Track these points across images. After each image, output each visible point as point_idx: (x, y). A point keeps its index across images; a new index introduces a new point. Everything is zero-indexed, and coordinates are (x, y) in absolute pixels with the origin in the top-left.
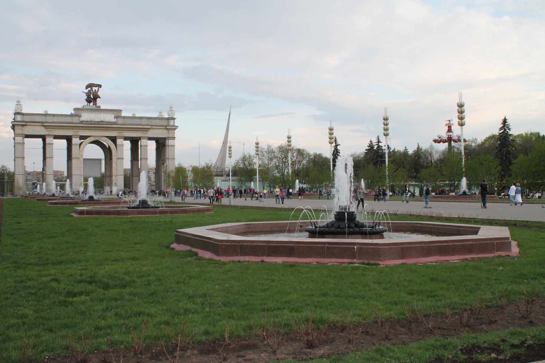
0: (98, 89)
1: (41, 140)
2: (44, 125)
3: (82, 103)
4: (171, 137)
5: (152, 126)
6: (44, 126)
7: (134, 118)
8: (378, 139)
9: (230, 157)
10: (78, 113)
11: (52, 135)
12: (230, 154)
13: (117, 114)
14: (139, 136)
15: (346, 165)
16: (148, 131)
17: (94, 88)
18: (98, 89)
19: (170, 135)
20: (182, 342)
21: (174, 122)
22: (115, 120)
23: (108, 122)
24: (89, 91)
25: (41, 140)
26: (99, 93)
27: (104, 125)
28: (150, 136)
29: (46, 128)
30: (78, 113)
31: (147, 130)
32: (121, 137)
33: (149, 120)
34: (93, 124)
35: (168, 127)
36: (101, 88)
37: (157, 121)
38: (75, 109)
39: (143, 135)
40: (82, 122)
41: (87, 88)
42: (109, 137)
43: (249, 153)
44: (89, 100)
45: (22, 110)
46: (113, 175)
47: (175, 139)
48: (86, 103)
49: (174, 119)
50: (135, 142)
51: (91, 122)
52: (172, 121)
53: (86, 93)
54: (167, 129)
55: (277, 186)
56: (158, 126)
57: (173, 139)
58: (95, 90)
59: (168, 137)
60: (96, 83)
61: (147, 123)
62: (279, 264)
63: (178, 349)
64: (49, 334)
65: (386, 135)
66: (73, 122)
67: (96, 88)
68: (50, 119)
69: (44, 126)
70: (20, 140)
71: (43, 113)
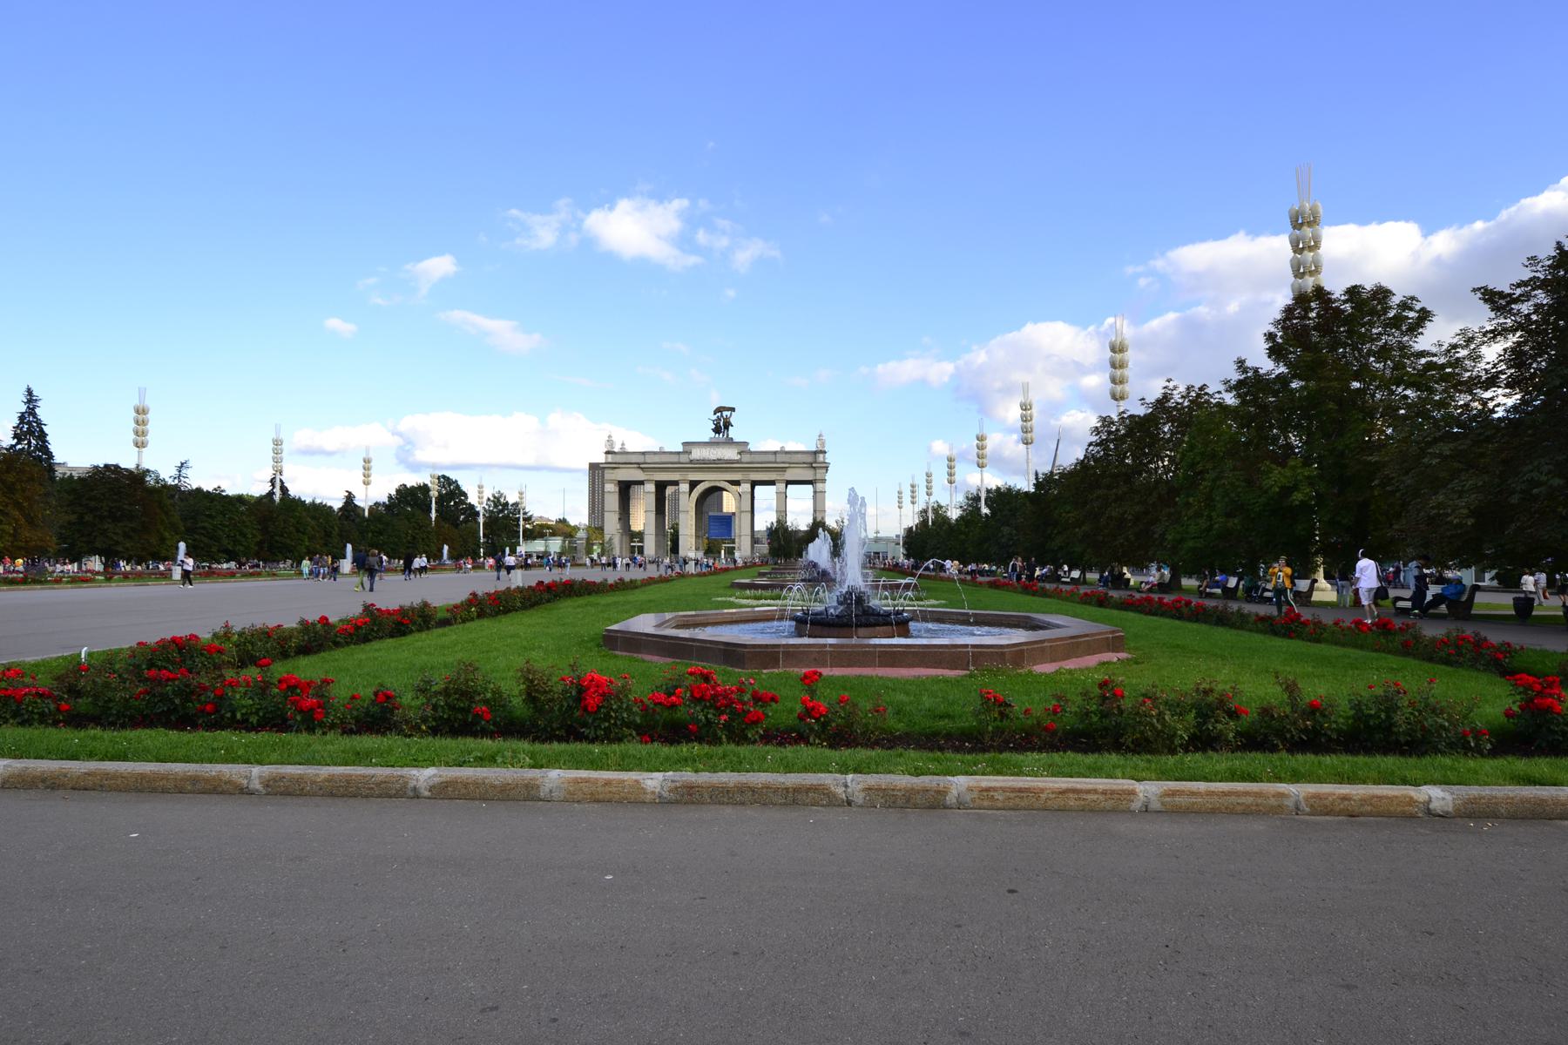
0: (731, 415)
1: (757, 487)
2: (639, 466)
3: (707, 434)
6: (642, 468)
8: (31, 411)
9: (913, 503)
10: (688, 448)
13: (742, 449)
16: (785, 471)
17: (725, 413)
18: (731, 415)
21: (824, 458)
25: (757, 487)
26: (732, 420)
30: (688, 448)
31: (784, 469)
35: (814, 465)
38: (685, 444)
39: (778, 478)
40: (691, 462)
41: (715, 414)
42: (699, 482)
44: (717, 430)
48: (714, 433)
49: (825, 452)
51: (704, 461)
52: (821, 456)
66: (681, 461)
67: (728, 413)
68: (649, 459)
69: (642, 468)
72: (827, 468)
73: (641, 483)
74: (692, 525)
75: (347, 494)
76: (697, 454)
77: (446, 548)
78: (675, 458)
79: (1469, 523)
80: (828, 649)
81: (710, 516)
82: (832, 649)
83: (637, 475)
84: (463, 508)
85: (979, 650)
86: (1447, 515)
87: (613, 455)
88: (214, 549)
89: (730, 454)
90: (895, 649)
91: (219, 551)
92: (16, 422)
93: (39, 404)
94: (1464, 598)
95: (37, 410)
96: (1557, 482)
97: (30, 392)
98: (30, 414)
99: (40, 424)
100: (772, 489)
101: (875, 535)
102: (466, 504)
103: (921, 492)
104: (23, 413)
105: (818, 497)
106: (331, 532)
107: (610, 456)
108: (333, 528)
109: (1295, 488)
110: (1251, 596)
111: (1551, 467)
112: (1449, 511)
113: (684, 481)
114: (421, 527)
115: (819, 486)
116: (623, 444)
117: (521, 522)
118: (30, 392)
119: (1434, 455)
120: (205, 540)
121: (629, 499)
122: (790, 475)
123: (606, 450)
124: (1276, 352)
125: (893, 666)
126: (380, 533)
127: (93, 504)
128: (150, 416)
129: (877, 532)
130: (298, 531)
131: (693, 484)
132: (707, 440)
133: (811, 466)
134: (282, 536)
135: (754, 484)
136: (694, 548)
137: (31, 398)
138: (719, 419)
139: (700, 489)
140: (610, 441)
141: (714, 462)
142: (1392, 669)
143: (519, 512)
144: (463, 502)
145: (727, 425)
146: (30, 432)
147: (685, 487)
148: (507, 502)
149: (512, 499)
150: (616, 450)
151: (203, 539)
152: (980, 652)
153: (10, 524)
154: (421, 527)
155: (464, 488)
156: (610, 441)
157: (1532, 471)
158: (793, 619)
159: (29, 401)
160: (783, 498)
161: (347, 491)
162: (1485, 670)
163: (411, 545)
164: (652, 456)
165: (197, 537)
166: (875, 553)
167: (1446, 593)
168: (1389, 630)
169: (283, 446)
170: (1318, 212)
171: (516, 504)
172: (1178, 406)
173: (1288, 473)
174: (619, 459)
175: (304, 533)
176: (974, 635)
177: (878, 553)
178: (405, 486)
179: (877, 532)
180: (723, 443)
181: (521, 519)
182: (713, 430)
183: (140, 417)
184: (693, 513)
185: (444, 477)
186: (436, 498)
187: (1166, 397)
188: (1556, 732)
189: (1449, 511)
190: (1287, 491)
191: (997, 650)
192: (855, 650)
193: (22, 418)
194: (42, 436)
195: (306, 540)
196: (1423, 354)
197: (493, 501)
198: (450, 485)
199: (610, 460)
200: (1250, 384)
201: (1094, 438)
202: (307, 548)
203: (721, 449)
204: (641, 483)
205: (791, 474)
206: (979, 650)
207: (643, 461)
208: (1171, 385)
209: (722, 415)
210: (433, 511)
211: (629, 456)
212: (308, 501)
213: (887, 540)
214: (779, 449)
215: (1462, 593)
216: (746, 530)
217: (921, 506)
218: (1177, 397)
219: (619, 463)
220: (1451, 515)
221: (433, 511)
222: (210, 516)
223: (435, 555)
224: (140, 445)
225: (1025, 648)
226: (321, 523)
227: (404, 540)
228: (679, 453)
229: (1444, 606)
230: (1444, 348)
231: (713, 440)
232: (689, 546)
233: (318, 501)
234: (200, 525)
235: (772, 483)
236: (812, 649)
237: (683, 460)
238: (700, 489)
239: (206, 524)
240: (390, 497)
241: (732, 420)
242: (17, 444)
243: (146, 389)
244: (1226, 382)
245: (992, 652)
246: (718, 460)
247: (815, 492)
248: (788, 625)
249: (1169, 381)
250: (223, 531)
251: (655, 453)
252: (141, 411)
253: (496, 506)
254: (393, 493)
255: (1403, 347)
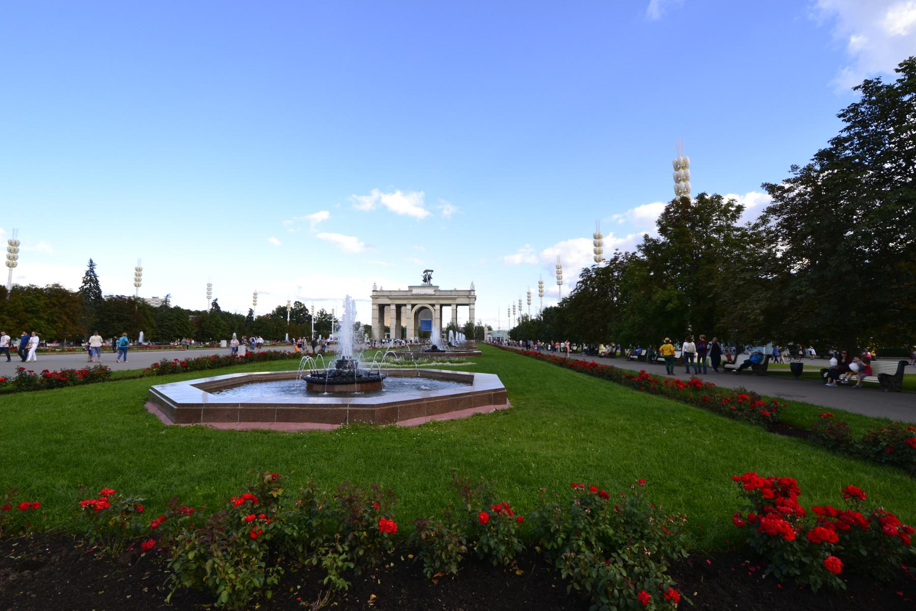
2: (388, 297)
3: (420, 282)
8: (92, 270)
12: (514, 311)
15: (509, 309)
17: (429, 273)
19: (471, 302)
22: (433, 293)
26: (432, 276)
30: (410, 289)
31: (455, 299)
38: (409, 287)
40: (412, 295)
42: (416, 304)
44: (425, 281)
51: (418, 295)
52: (473, 292)
62: (255, 355)
63: (42, 348)
64: (729, 526)
65: (10, 265)
67: (430, 273)
73: (389, 305)
76: (415, 291)
77: (287, 334)
78: (405, 294)
79: (761, 319)
80: (240, 407)
85: (387, 407)
86: (748, 314)
88: (172, 335)
89: (430, 291)
92: (84, 275)
93: (95, 267)
94: (762, 363)
95: (94, 270)
96: (812, 291)
97: (91, 261)
98: (91, 271)
99: (95, 276)
104: (88, 271)
105: (472, 311)
109: (669, 301)
110: (651, 360)
111: (808, 283)
112: (750, 311)
113: (409, 304)
115: (472, 306)
117: (333, 323)
118: (91, 261)
119: (741, 279)
120: (167, 331)
121: (384, 312)
122: (458, 301)
124: (663, 231)
125: (287, 421)
126: (260, 328)
127: (108, 313)
128: (143, 272)
129: (499, 328)
131: (413, 306)
133: (468, 297)
137: (92, 264)
138: (426, 275)
139: (416, 308)
140: (375, 285)
141: (423, 295)
142: (687, 421)
144: (306, 314)
145: (430, 278)
146: (91, 280)
147: (409, 307)
150: (378, 289)
153: (62, 323)
155: (307, 308)
156: (375, 285)
157: (796, 285)
159: (91, 266)
162: (756, 424)
167: (752, 359)
168: (698, 387)
170: (687, 162)
171: (331, 315)
172: (621, 262)
173: (666, 292)
174: (379, 294)
176: (422, 390)
179: (499, 328)
183: (138, 273)
185: (298, 302)
187: (616, 259)
188: (793, 563)
189: (750, 311)
190: (665, 302)
191: (368, 409)
192: (259, 408)
193: (87, 274)
194: (97, 282)
196: (738, 229)
198: (301, 306)
199: (375, 294)
200: (650, 246)
201: (581, 279)
204: (405, 305)
207: (390, 295)
208: (618, 252)
210: (289, 318)
213: (504, 332)
214: (453, 289)
215: (761, 360)
217: (517, 316)
218: (621, 259)
220: (751, 313)
221: (289, 318)
222: (170, 320)
223: (134, 337)
224: (137, 286)
228: (406, 291)
229: (750, 367)
230: (751, 226)
232: (411, 336)
233: (238, 313)
234: (165, 324)
235: (450, 305)
237: (409, 295)
238: (416, 308)
239: (168, 324)
242: (85, 285)
244: (639, 246)
247: (470, 309)
248: (301, 384)
249: (617, 250)
252: (139, 270)
253: (321, 316)
254: (275, 310)
255: (729, 226)
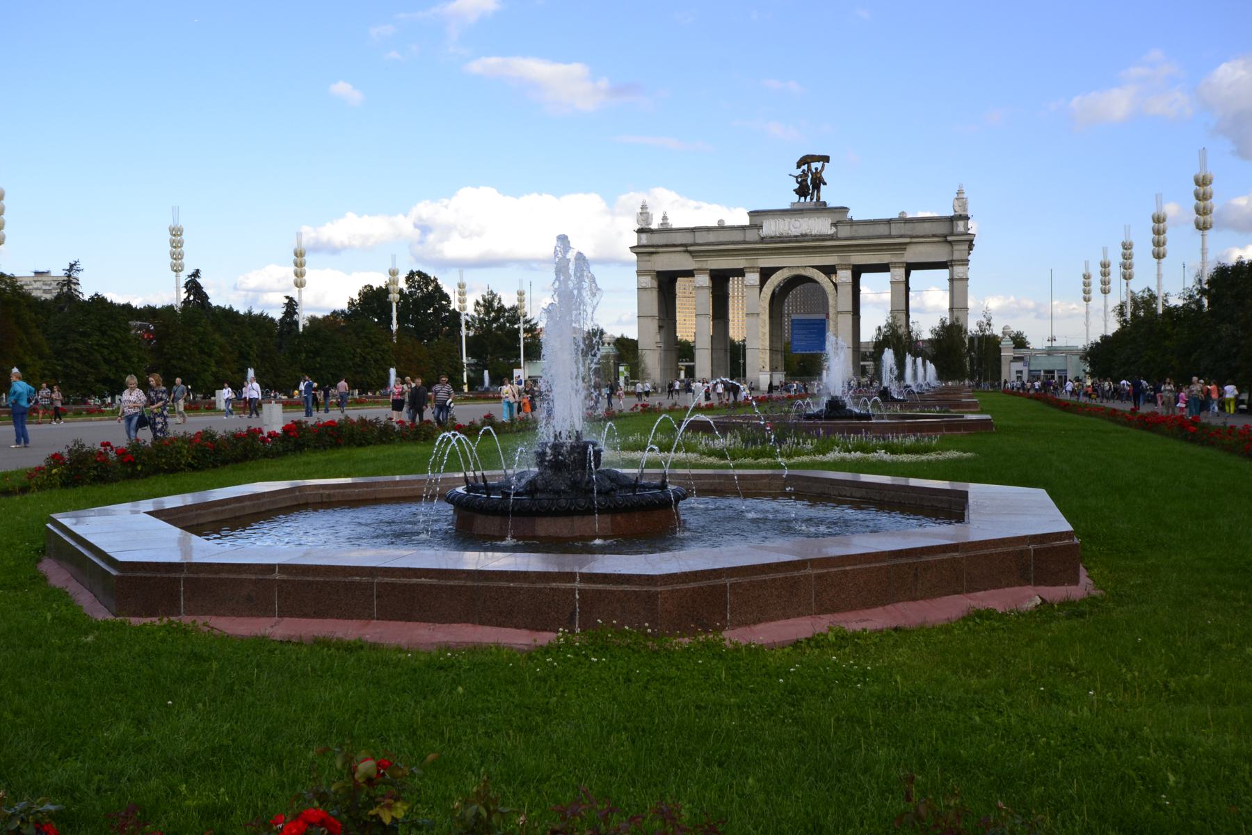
2: (686, 249)
3: (787, 197)
4: (958, 261)
5: (912, 237)
6: (690, 252)
7: (722, 228)
10: (757, 220)
11: (707, 269)
13: (838, 217)
14: (886, 261)
17: (814, 165)
18: (823, 167)
20: (1147, 744)
21: (966, 226)
22: (832, 231)
23: (815, 236)
24: (804, 171)
26: (825, 175)
27: (808, 241)
28: (909, 261)
29: (693, 257)
30: (757, 220)
31: (902, 247)
32: (845, 265)
33: (909, 226)
34: (786, 243)
35: (949, 238)
36: (828, 162)
37: (927, 225)
39: (894, 260)
40: (763, 240)
41: (799, 167)
43: (1149, 290)
44: (802, 191)
45: (650, 224)
46: (768, 351)
47: (967, 265)
49: (966, 218)
50: (720, 280)
51: (781, 239)
52: (961, 224)
53: (797, 177)
54: (950, 243)
55: (44, 385)
56: (929, 237)
57: (963, 265)
58: (816, 169)
59: (952, 261)
60: (817, 153)
61: (902, 232)
66: (747, 239)
67: (818, 165)
68: (700, 238)
69: (690, 252)
70: (646, 283)
71: (716, 225)
72: (971, 245)
73: (689, 274)
74: (764, 334)
75: (287, 301)
76: (771, 228)
77: (486, 372)
78: (738, 236)
81: (792, 321)
82: (284, 577)
83: (686, 263)
84: (446, 316)
85: (600, 586)
87: (649, 235)
88: (91, 378)
89: (820, 225)
90: (414, 580)
91: (97, 381)
100: (884, 278)
101: (1049, 344)
102: (448, 311)
103: (1115, 272)
106: (248, 354)
107: (644, 236)
108: (250, 346)
113: (752, 270)
114: (373, 344)
115: (959, 270)
116: (665, 218)
117: (522, 335)
122: (912, 255)
123: (637, 227)
129: (1053, 339)
130: (202, 352)
131: (766, 274)
132: (787, 206)
133: (946, 240)
134: (180, 359)
135: (909, 267)
136: (767, 368)
138: (804, 174)
139: (775, 280)
140: (644, 213)
141: (796, 239)
143: (519, 319)
145: (818, 182)
147: (753, 278)
148: (502, 307)
149: (508, 301)
150: (654, 226)
151: (76, 365)
152: (599, 591)
154: (373, 344)
155: (446, 290)
156: (644, 213)
158: (450, 500)
160: (904, 290)
161: (287, 297)
163: (359, 369)
164: (705, 233)
165: (69, 362)
166: (1046, 372)
169: (1133, 270)
171: (514, 309)
174: (657, 239)
175: (210, 355)
177: (1053, 372)
178: (371, 287)
179: (1053, 339)
180: (810, 210)
181: (522, 331)
182: (797, 191)
184: (766, 317)
185: (419, 273)
186: (397, 303)
195: (213, 363)
197: (484, 306)
198: (427, 285)
199: (644, 241)
202: (214, 375)
203: (806, 219)
205: (914, 254)
206: (600, 586)
209: (809, 169)
210: (394, 321)
211: (673, 235)
212: (242, 311)
213: (1069, 351)
214: (896, 216)
216: (845, 341)
219: (658, 246)
221: (394, 321)
222: (84, 334)
225: (728, 582)
226: (236, 341)
227: (350, 363)
228: (743, 228)
231: (796, 207)
233: (256, 311)
235: (884, 268)
236: (244, 576)
238: (775, 280)
239: (79, 345)
240: (351, 303)
241: (825, 175)
243: (1130, 226)
245: (626, 593)
246: (802, 235)
247: (952, 280)
250: (102, 353)
251: (708, 229)
253: (487, 313)
